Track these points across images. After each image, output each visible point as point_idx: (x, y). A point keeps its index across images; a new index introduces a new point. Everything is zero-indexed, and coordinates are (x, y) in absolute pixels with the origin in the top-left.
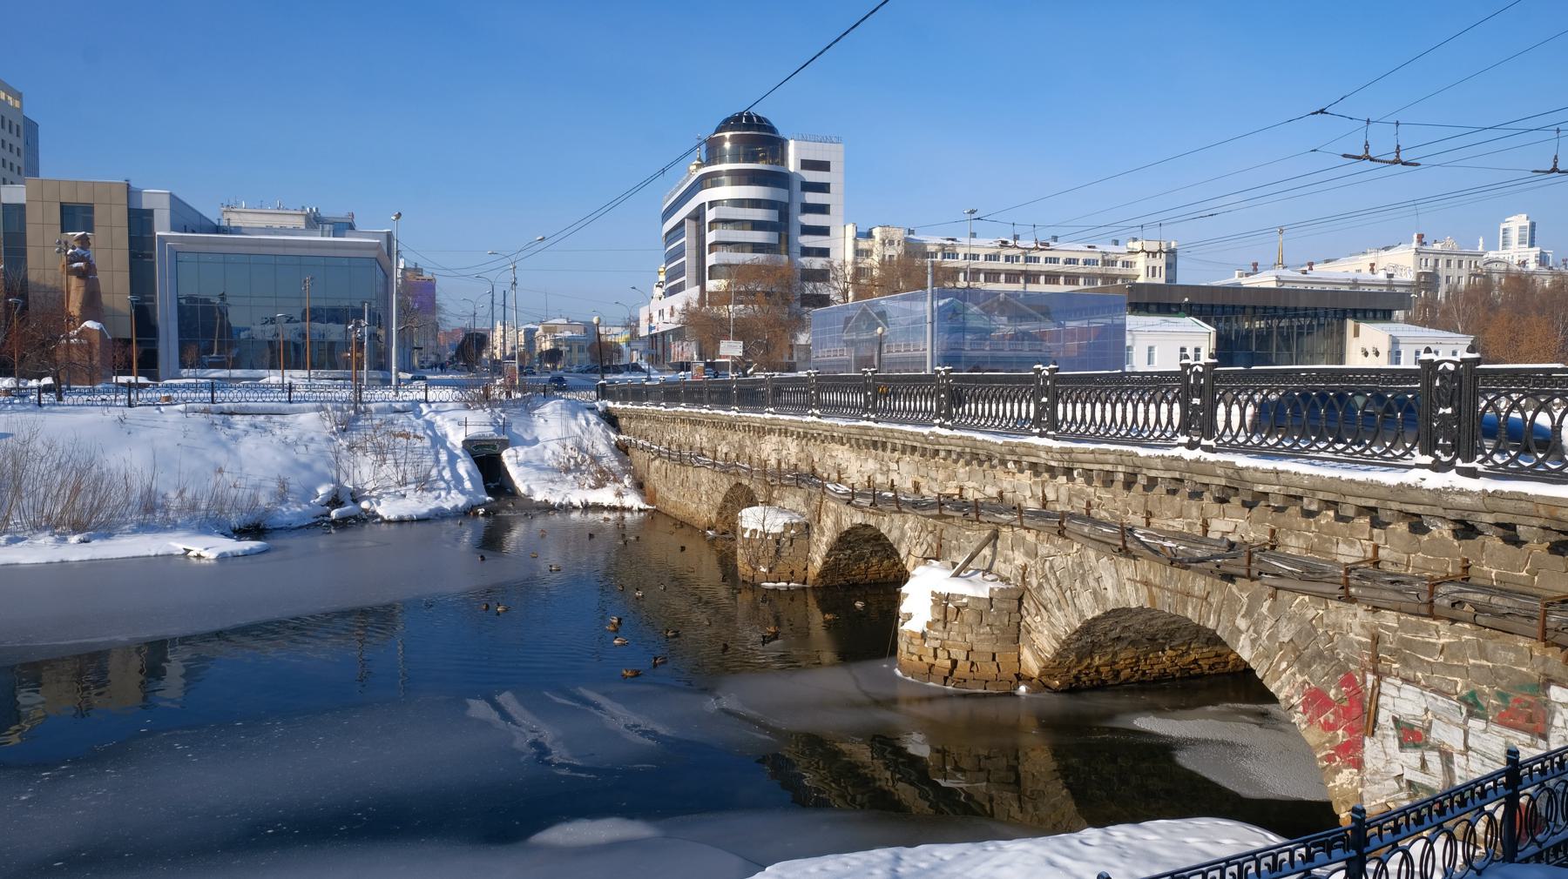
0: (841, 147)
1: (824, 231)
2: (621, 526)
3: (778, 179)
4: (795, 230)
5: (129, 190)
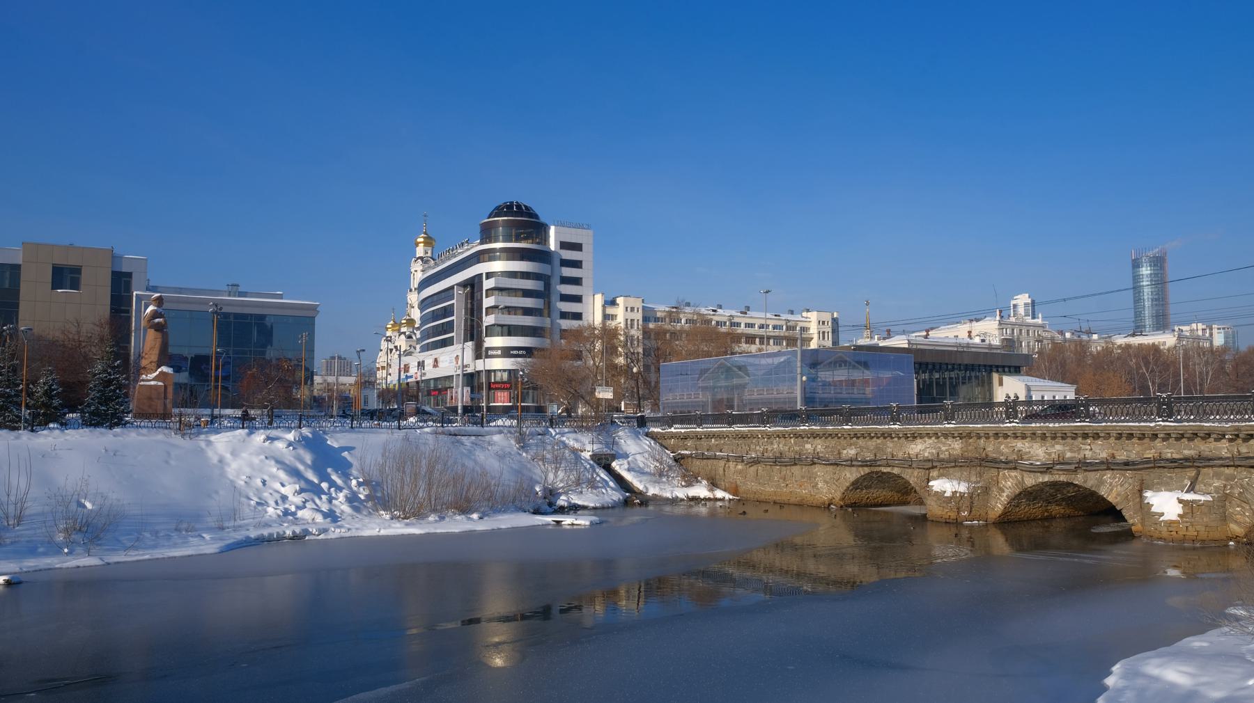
0: (590, 232)
1: (577, 299)
2: (713, 514)
3: (542, 256)
4: (554, 297)
5: (115, 258)
